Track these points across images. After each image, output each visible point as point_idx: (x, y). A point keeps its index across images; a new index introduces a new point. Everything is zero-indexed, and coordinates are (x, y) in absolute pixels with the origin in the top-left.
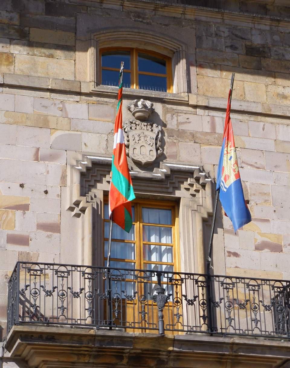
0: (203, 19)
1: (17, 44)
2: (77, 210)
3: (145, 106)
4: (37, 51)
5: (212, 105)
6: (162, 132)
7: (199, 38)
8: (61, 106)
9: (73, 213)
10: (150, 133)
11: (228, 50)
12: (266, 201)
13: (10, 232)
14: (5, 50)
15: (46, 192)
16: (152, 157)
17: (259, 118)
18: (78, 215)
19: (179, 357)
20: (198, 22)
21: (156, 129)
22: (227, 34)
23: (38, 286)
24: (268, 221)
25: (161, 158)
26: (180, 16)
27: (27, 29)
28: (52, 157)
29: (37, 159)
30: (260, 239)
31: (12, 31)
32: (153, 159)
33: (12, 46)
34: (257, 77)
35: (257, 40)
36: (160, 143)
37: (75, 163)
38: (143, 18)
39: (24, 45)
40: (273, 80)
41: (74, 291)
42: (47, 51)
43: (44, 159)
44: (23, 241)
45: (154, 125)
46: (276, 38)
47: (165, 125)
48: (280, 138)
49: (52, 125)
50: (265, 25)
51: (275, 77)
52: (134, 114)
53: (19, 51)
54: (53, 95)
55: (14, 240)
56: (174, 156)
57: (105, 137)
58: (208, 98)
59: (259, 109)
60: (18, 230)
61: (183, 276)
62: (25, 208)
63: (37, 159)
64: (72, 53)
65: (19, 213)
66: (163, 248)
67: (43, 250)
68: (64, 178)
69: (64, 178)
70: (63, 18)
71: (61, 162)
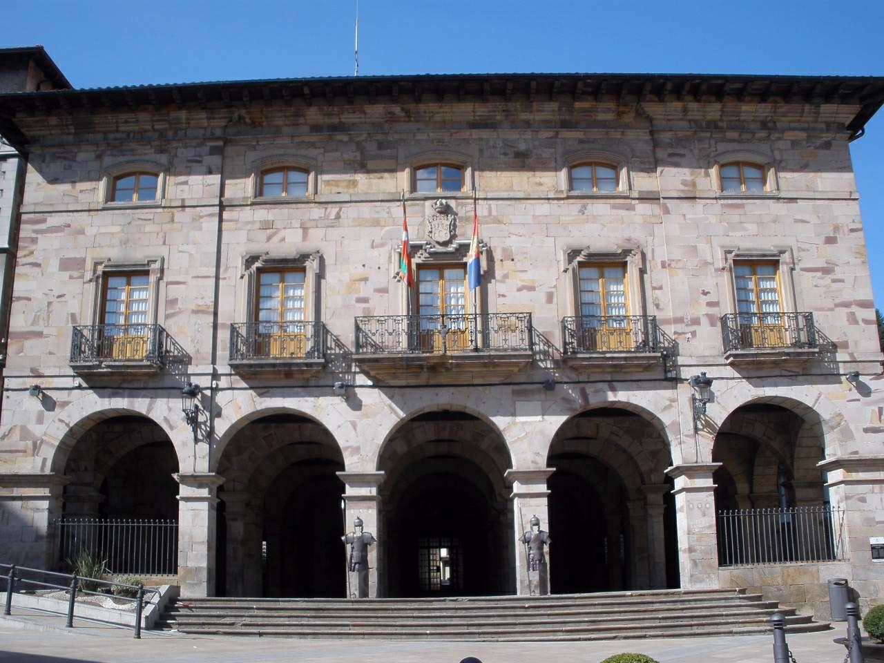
0: (485, 137)
1: (360, 173)
2: (398, 278)
3: (441, 204)
4: (372, 176)
5: (489, 197)
6: (455, 220)
7: (481, 151)
8: (388, 210)
9: (396, 280)
10: (446, 221)
11: (502, 157)
12: (525, 258)
13: (357, 296)
14: (352, 178)
15: (379, 268)
16: (447, 238)
17: (523, 201)
18: (399, 281)
19: (458, 365)
20: (481, 139)
21: (450, 217)
22: (501, 145)
23: (384, 330)
24: (526, 271)
25: (453, 237)
26: (467, 137)
27: (365, 162)
28: (382, 245)
29: (373, 247)
30: (520, 284)
31: (356, 165)
32: (448, 239)
33: (356, 175)
34: (521, 173)
35: (522, 147)
36: (453, 227)
37: (396, 247)
38: (443, 142)
39: (364, 173)
40: (533, 173)
41: (389, 331)
42: (378, 175)
43: (377, 247)
44: (365, 300)
45: (449, 215)
46: (537, 143)
47: (457, 214)
48: (537, 214)
49: (382, 223)
50: (528, 135)
51: (534, 171)
52: (435, 209)
53: (360, 177)
54: (383, 203)
55: (359, 300)
56: (463, 235)
57: (417, 228)
58: (486, 192)
59: (521, 195)
60: (362, 294)
61: (386, 318)
62: (366, 279)
63: (373, 247)
64: (394, 174)
65: (363, 283)
66: (459, 295)
67: (379, 306)
68: (390, 257)
69: (390, 257)
70: (389, 151)
71: (387, 248)
